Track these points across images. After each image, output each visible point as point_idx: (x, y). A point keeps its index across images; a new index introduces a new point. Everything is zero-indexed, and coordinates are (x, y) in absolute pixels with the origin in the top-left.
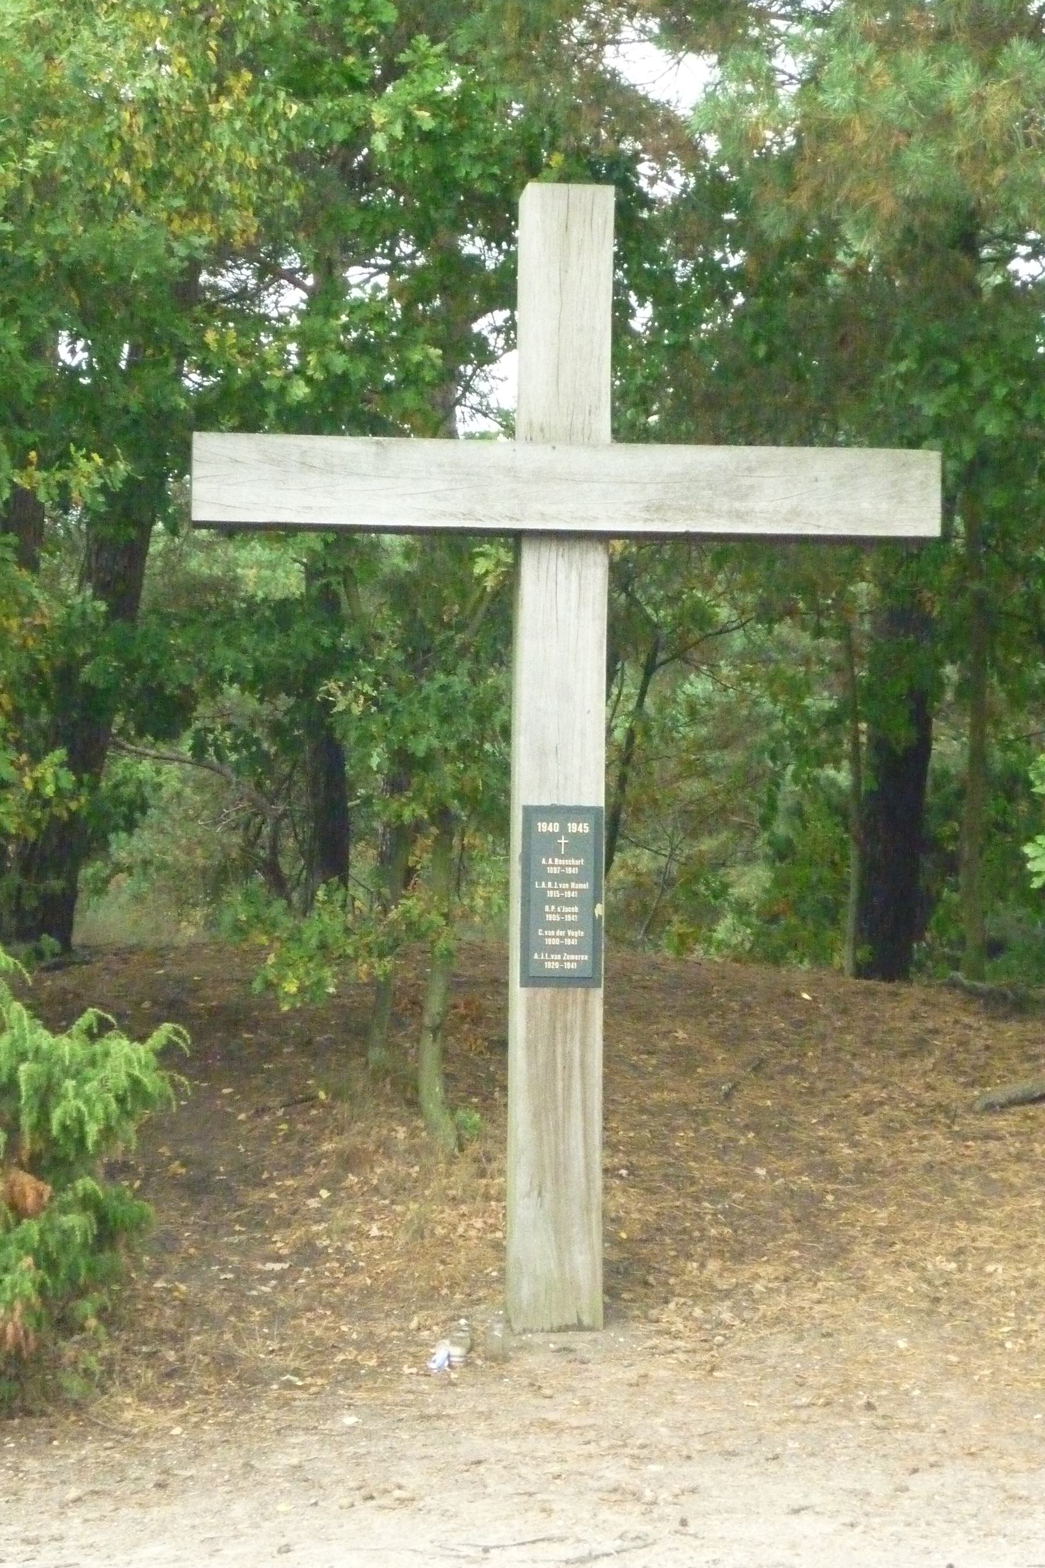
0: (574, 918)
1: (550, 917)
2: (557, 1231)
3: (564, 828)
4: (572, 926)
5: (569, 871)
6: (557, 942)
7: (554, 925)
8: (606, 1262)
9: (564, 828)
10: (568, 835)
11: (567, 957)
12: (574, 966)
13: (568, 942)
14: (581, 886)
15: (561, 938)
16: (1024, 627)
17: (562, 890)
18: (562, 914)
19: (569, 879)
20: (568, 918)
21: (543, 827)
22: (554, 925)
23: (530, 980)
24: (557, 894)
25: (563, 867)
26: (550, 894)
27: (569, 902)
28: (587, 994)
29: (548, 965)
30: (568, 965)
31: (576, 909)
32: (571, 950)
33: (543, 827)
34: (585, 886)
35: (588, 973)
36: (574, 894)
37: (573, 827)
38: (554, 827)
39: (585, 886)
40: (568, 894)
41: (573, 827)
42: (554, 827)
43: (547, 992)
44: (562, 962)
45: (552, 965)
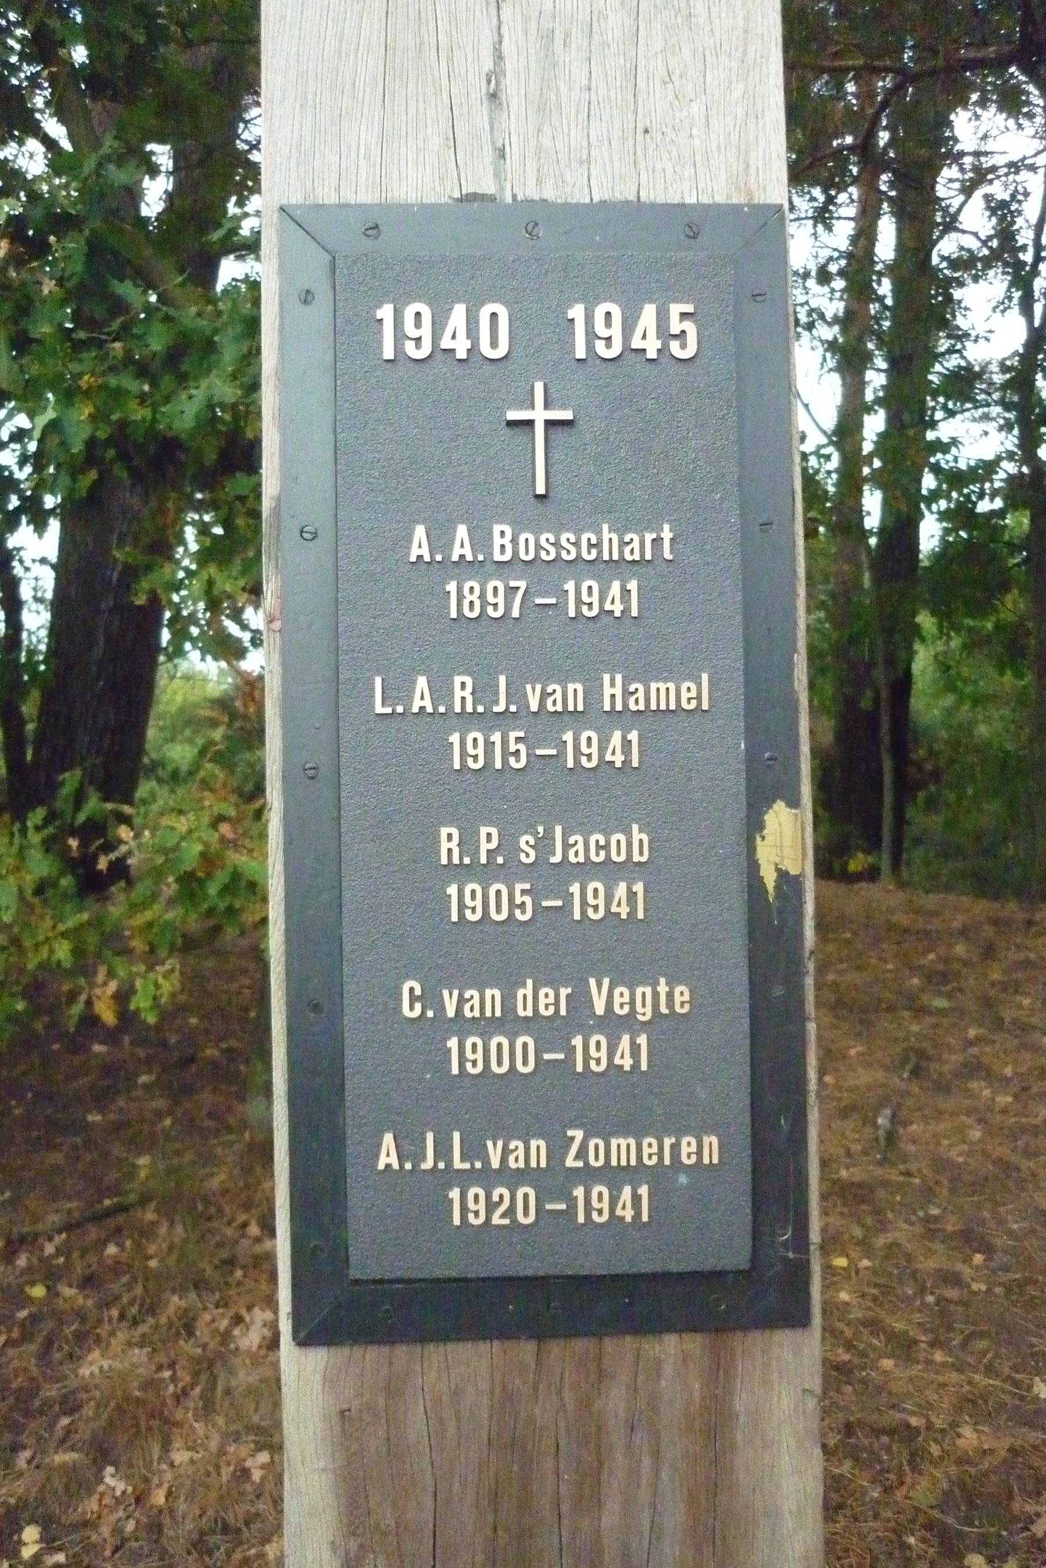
0: (624, 898)
1: (468, 901)
2: (754, 1239)
3: (542, 339)
4: (621, 951)
5: (584, 596)
6: (520, 1054)
7: (499, 954)
8: (825, 1361)
9: (542, 339)
10: (568, 371)
11: (586, 1148)
12: (631, 1204)
13: (593, 1053)
14: (662, 693)
15: (550, 1031)
16: (966, 707)
17: (546, 723)
18: (551, 876)
19: (590, 648)
20: (590, 900)
21: (407, 328)
22: (499, 954)
23: (345, 1311)
24: (514, 749)
25: (546, 572)
26: (468, 748)
27: (591, 796)
28: (719, 1372)
29: (470, 1206)
30: (595, 1203)
31: (636, 843)
32: (619, 1103)
33: (407, 328)
34: (691, 693)
35: (727, 1246)
36: (619, 747)
37: (599, 327)
38: (479, 329)
39: (691, 693)
40: (583, 747)
41: (599, 327)
42: (479, 329)
43: (465, 1370)
44: (552, 1181)
45: (493, 1203)
